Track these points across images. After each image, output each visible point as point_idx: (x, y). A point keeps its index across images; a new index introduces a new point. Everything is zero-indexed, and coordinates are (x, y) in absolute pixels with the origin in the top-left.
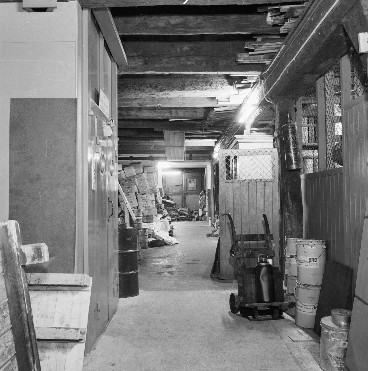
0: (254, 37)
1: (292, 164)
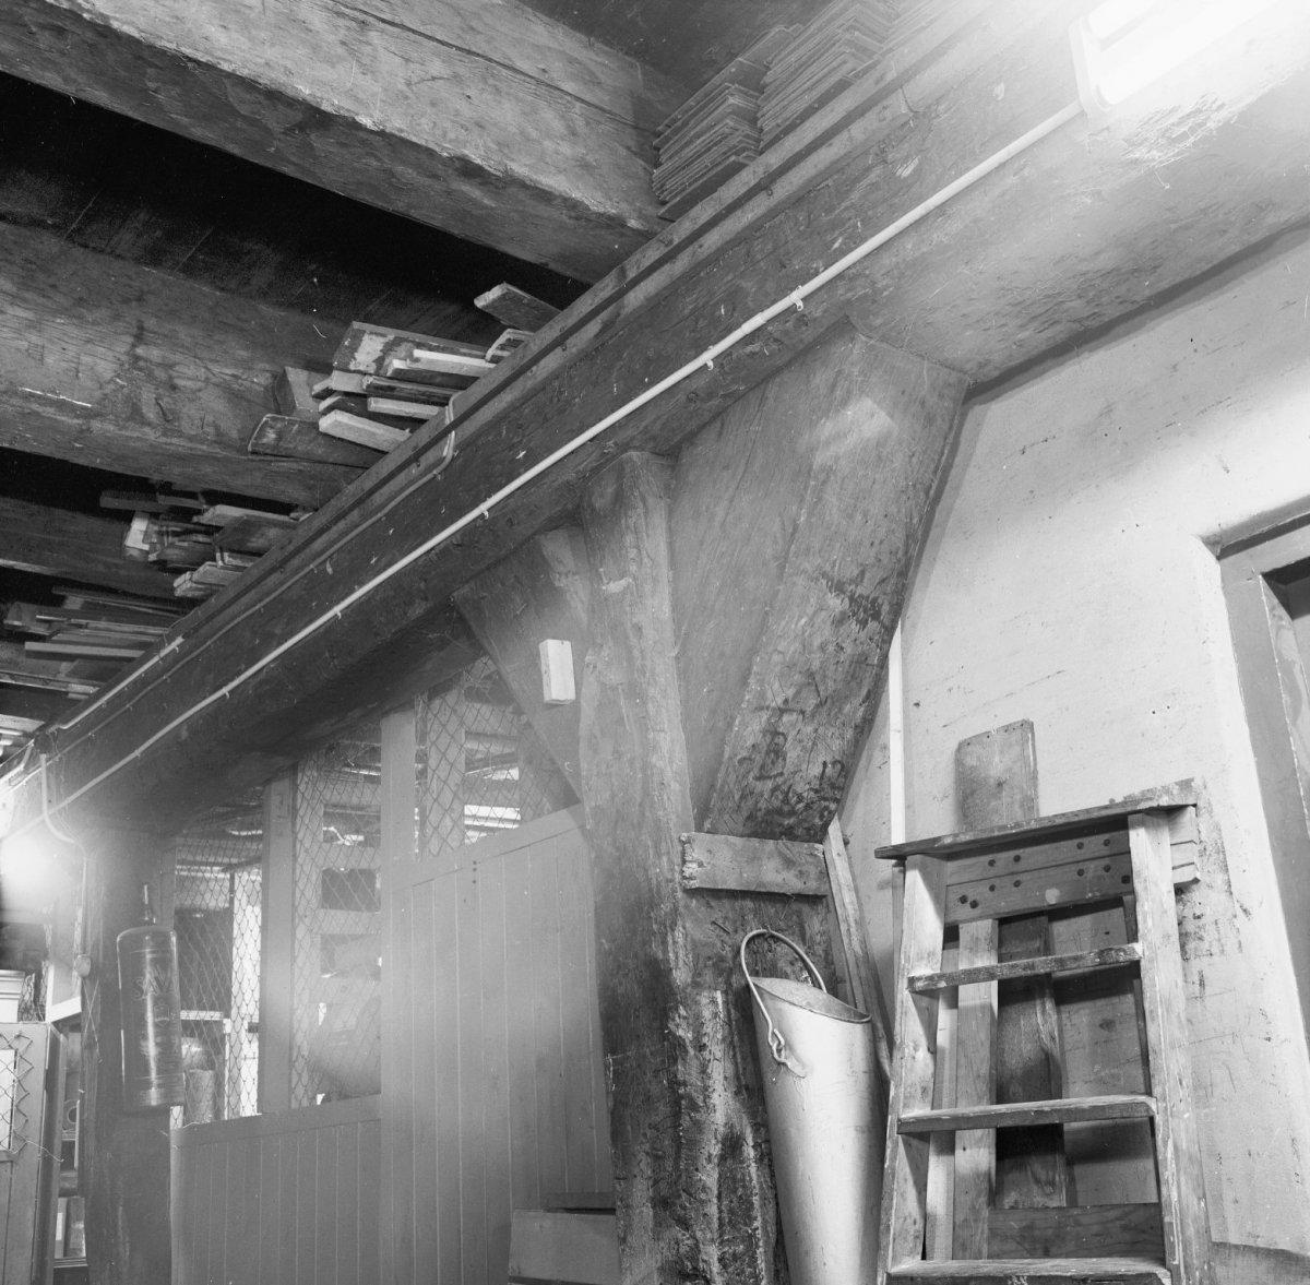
0: (56, 591)
1: (148, 1085)
